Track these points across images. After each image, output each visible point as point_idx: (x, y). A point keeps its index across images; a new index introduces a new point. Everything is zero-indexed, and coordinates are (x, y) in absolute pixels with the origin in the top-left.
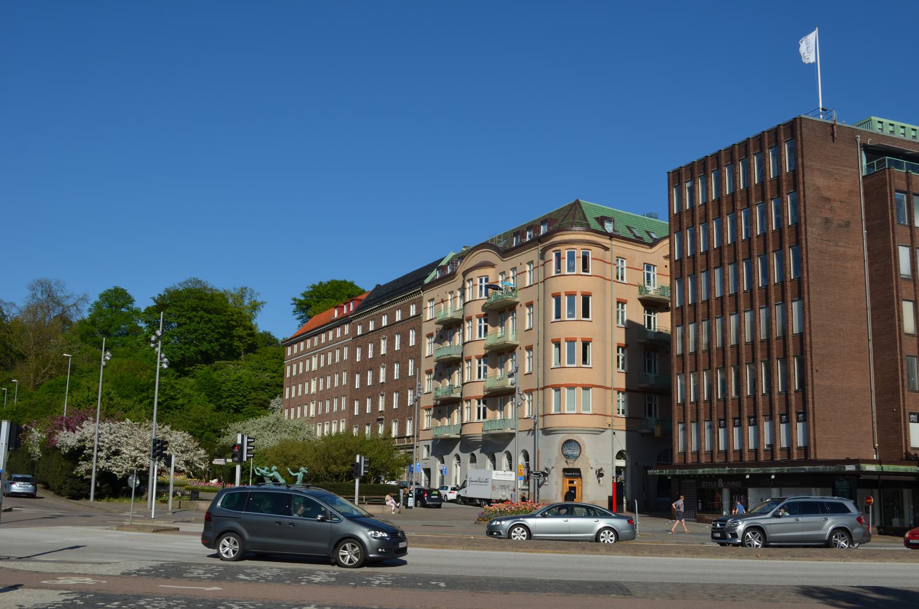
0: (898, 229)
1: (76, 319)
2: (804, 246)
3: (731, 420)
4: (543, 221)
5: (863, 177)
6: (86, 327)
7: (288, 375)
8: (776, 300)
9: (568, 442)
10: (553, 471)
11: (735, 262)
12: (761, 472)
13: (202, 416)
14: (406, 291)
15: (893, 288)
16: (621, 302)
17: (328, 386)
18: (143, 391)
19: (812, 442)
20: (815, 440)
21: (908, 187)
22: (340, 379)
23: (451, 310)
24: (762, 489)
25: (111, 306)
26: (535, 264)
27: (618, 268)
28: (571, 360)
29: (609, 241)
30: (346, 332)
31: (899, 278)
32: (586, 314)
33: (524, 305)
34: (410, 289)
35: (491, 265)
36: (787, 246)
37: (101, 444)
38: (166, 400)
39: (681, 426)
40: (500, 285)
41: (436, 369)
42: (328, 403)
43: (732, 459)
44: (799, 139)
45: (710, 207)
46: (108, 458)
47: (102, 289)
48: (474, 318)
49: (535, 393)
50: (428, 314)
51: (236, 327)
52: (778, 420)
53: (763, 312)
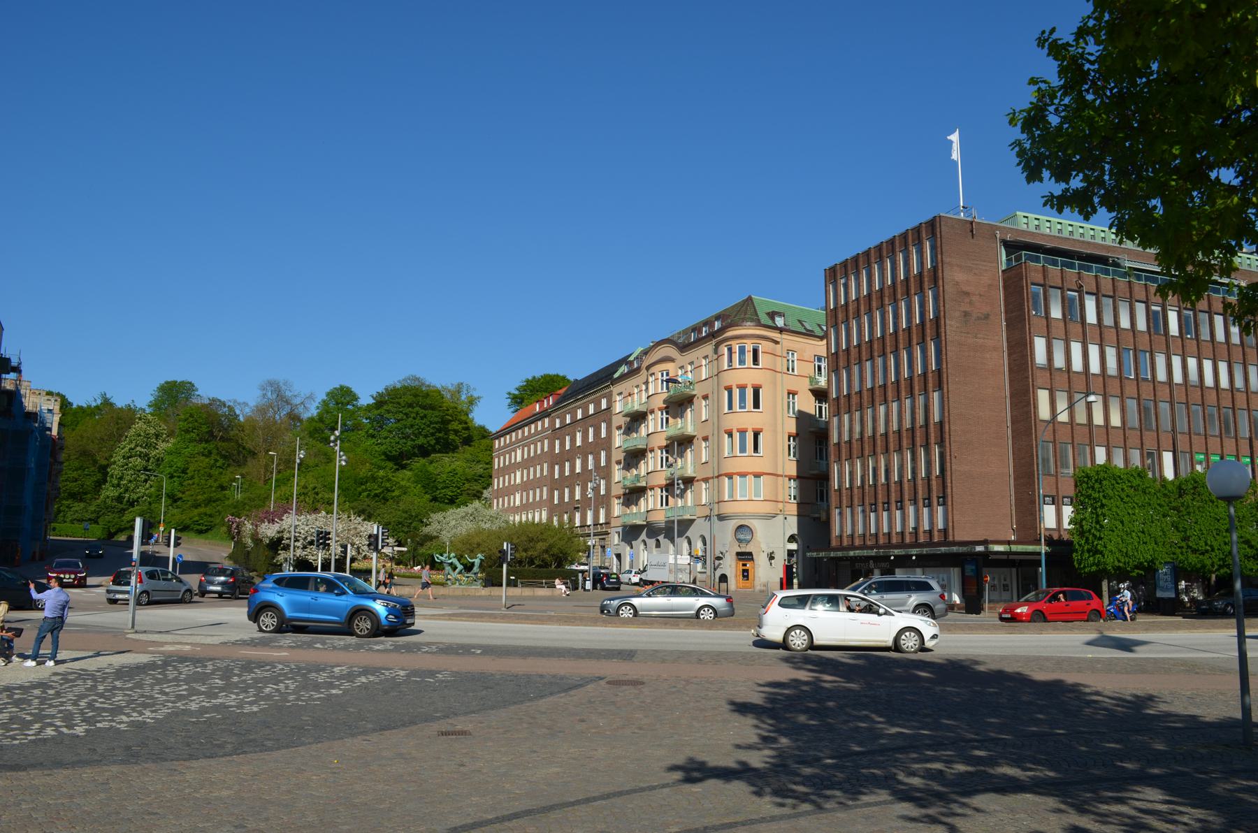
0: (1034, 321)
1: (306, 416)
2: (943, 338)
3: (881, 505)
4: (718, 317)
5: (1003, 271)
6: (314, 424)
7: (496, 467)
8: (920, 391)
9: (741, 527)
10: (727, 555)
11: (884, 354)
12: (903, 553)
13: (411, 507)
14: (598, 385)
15: (1028, 378)
16: (792, 393)
17: (531, 477)
18: (362, 484)
19: (950, 524)
20: (953, 522)
21: (1044, 279)
22: (542, 470)
23: (636, 404)
24: (908, 569)
25: (337, 404)
26: (710, 359)
27: (788, 360)
28: (743, 449)
29: (779, 335)
30: (546, 425)
31: (1034, 368)
32: (756, 405)
33: (700, 398)
34: (603, 383)
35: (671, 360)
36: (929, 339)
37: (297, 535)
38: (383, 492)
39: (837, 511)
40: (680, 380)
41: (624, 460)
42: (531, 492)
43: (881, 542)
44: (939, 236)
45: (862, 302)
46: (304, 548)
47: (329, 388)
48: (656, 410)
49: (710, 481)
50: (618, 407)
51: (452, 421)
52: (921, 504)
53: (908, 402)
